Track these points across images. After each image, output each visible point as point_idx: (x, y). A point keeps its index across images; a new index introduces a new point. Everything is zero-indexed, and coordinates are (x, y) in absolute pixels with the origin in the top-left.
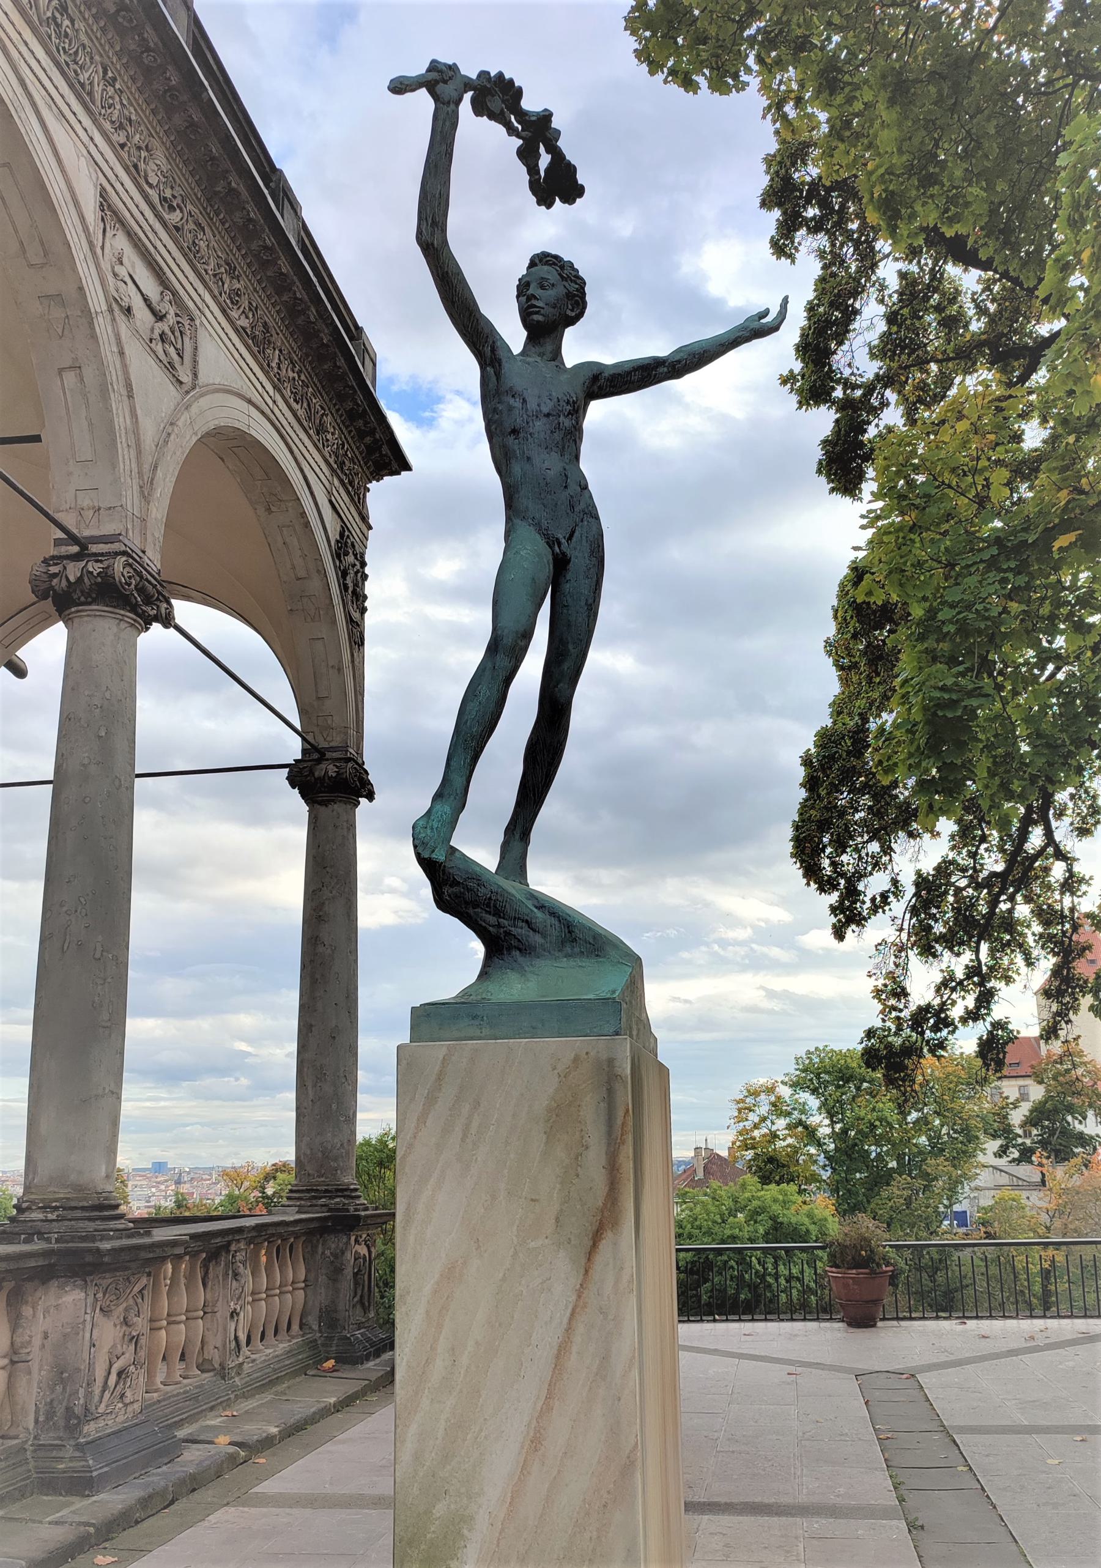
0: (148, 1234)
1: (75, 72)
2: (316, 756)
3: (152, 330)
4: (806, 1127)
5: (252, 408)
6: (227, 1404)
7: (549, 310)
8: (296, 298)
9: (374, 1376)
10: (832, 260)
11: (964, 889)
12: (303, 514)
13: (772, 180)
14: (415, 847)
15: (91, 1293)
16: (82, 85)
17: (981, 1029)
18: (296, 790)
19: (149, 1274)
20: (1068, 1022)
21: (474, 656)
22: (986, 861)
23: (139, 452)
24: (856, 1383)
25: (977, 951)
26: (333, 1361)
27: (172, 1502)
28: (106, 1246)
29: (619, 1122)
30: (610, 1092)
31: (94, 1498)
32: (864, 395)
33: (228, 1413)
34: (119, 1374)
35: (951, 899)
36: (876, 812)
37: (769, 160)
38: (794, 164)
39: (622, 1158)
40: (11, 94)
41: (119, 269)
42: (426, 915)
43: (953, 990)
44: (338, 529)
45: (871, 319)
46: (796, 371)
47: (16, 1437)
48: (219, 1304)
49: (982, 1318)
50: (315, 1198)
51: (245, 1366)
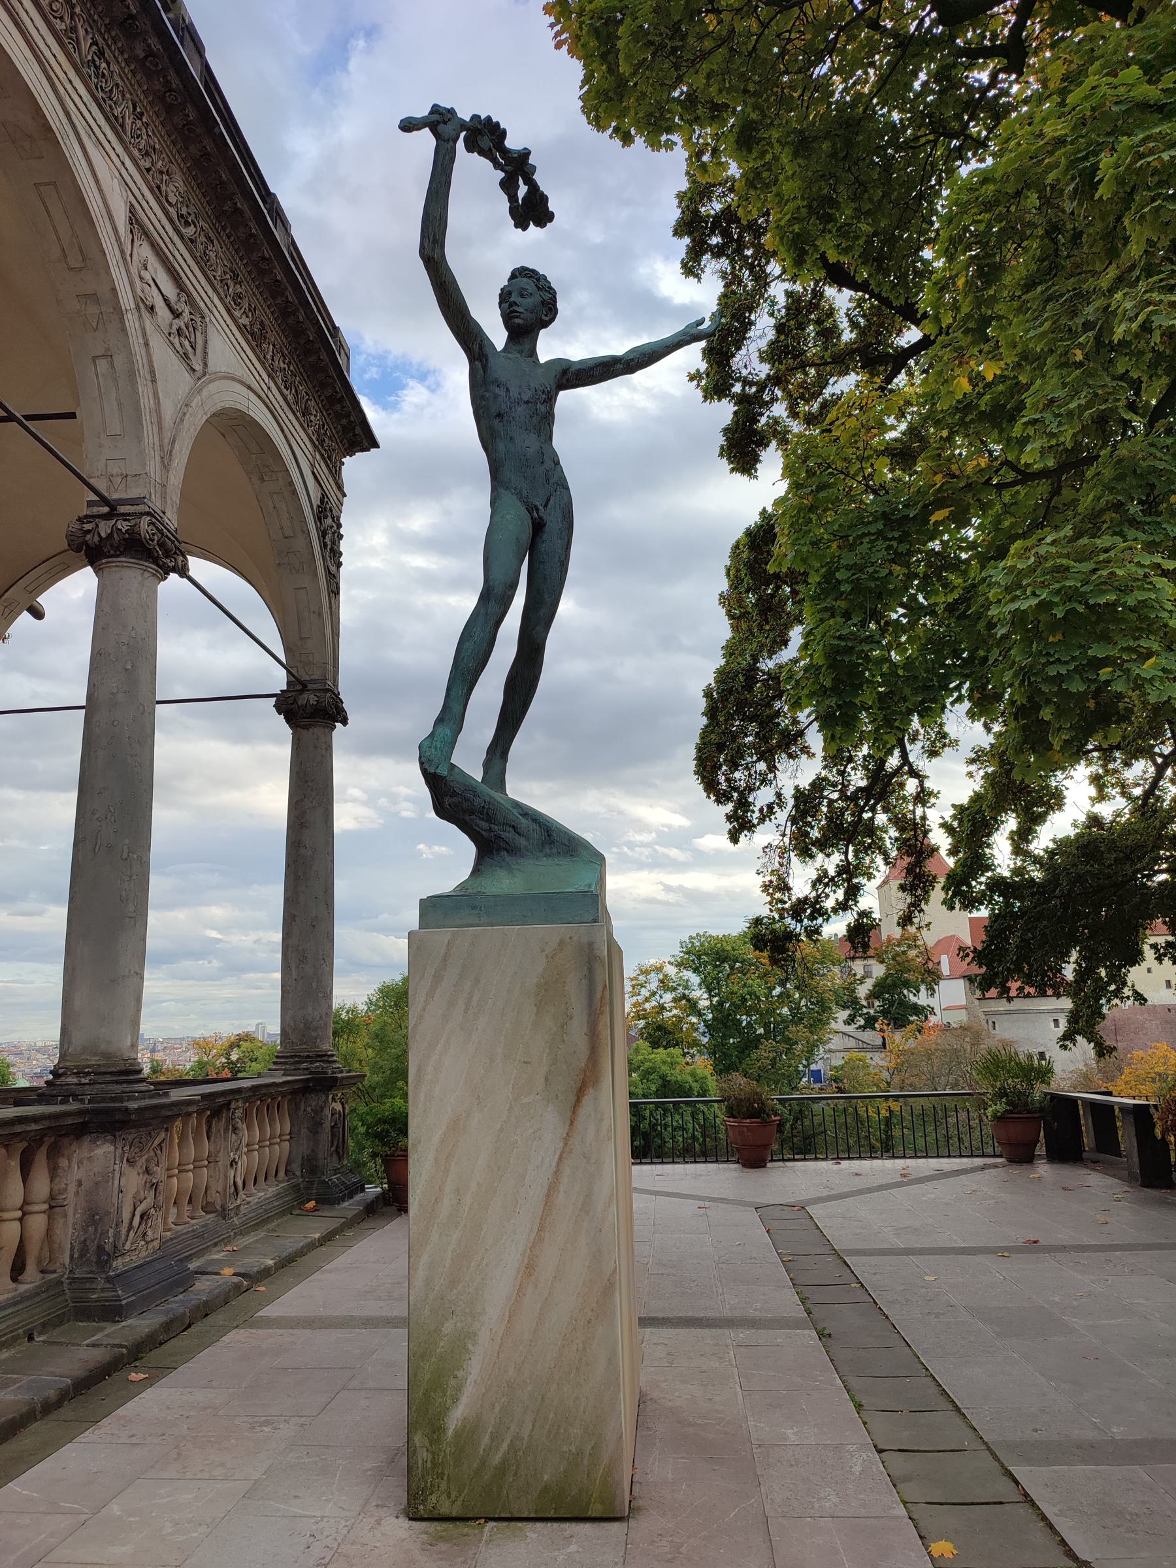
0: (166, 1095)
1: (110, 107)
2: (299, 687)
3: (171, 325)
4: (689, 1000)
5: (251, 393)
6: (228, 1241)
7: (527, 315)
8: (288, 302)
9: (350, 1215)
10: (731, 280)
11: (836, 801)
12: (291, 483)
13: (683, 212)
14: (421, 764)
15: (119, 1146)
16: (116, 118)
17: (849, 918)
18: (282, 716)
19: (167, 1130)
20: (921, 911)
21: (467, 602)
22: (853, 777)
23: (160, 428)
24: (757, 1215)
25: (846, 853)
26: (313, 1203)
27: (189, 1326)
28: (134, 1105)
29: (598, 995)
30: (591, 970)
31: (124, 1324)
32: (758, 391)
33: (230, 1248)
34: (142, 1216)
35: (825, 809)
36: (762, 737)
37: (681, 196)
38: (701, 199)
39: (601, 1027)
40: (58, 123)
41: (144, 274)
42: (382, 821)
43: (826, 885)
44: (319, 495)
45: (763, 328)
46: (702, 371)
47: (54, 1272)
48: (221, 1155)
49: (853, 1158)
50: (297, 1062)
51: (242, 1208)
